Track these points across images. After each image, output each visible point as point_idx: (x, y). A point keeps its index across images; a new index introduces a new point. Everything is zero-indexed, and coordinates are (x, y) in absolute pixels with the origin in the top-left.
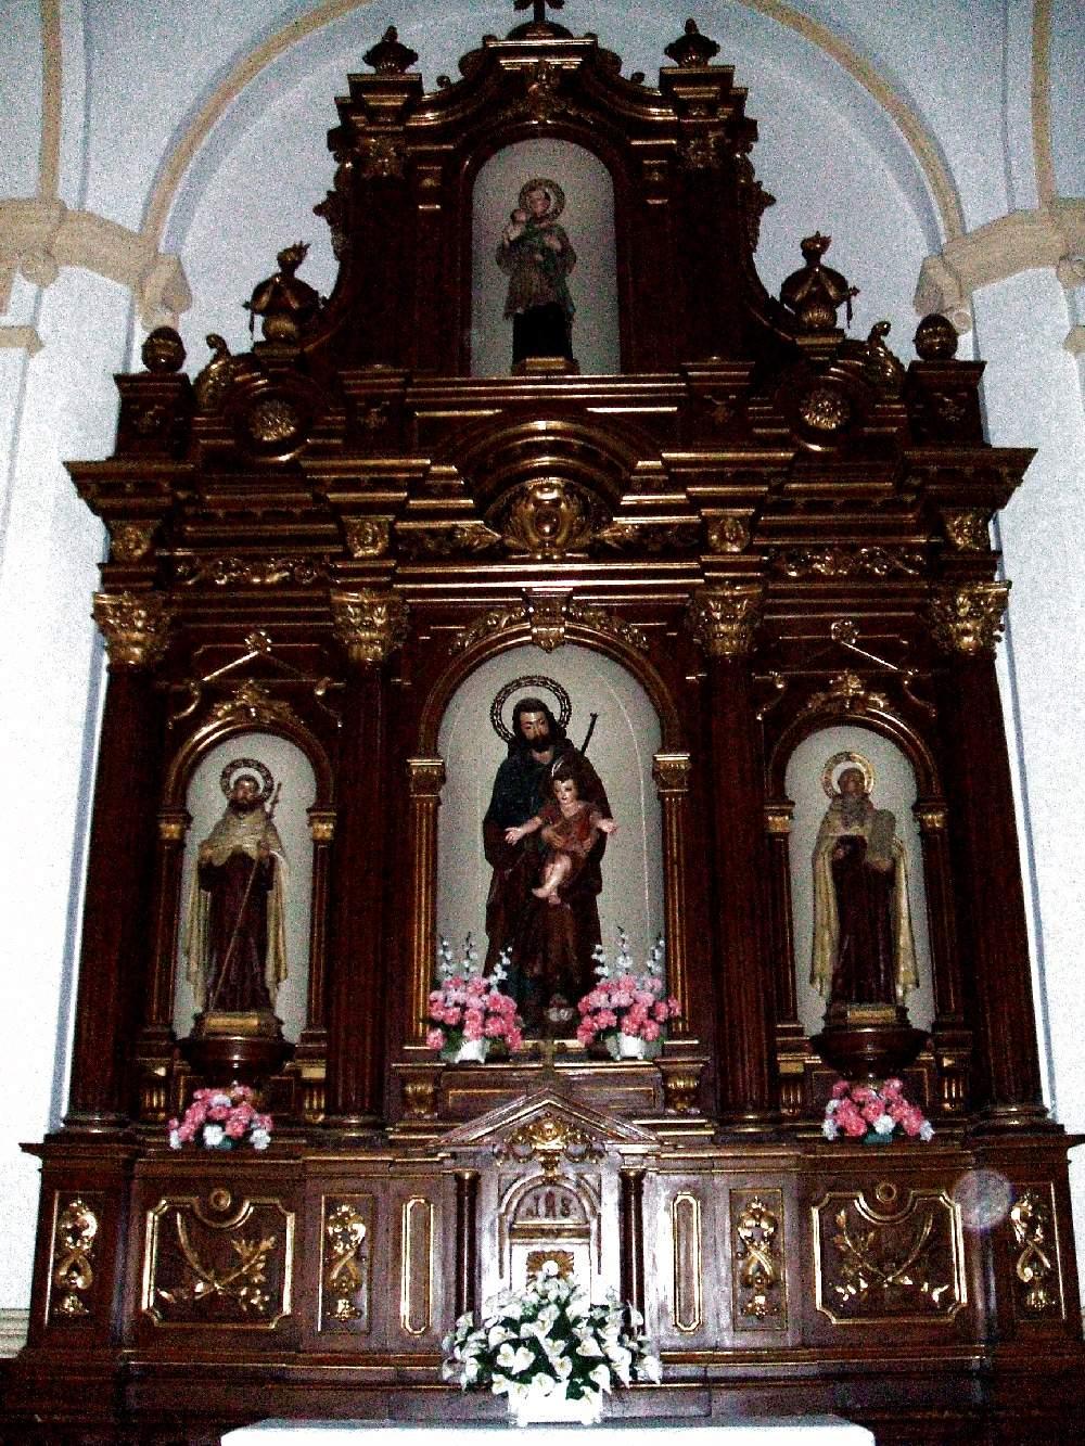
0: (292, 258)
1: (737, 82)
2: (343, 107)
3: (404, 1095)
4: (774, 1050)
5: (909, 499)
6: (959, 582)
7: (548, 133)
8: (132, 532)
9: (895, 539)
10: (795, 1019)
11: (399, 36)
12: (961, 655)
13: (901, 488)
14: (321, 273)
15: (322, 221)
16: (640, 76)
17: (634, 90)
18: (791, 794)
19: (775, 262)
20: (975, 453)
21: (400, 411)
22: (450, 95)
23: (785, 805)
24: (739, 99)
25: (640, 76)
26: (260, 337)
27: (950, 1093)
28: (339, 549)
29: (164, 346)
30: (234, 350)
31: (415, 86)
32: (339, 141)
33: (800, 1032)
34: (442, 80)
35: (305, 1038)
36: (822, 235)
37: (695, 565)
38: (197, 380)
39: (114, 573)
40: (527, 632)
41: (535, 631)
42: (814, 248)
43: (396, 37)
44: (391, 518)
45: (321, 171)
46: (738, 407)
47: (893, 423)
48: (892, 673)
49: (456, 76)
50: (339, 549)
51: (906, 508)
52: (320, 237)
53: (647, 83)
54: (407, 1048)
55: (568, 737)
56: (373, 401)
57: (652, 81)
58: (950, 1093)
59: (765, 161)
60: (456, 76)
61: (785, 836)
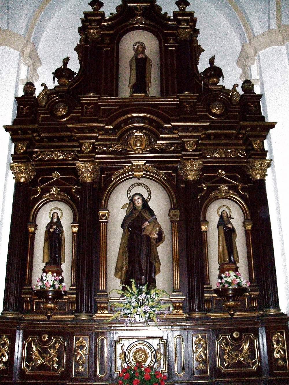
0: (66, 61)
2: (83, 21)
3: (97, 307)
4: (203, 292)
5: (241, 136)
7: (143, 29)
8: (20, 145)
9: (237, 147)
10: (209, 284)
12: (257, 180)
13: (239, 133)
14: (75, 66)
15: (76, 53)
16: (166, 13)
18: (207, 219)
19: (203, 66)
20: (261, 123)
21: (97, 107)
22: (113, 17)
23: (206, 222)
24: (195, 21)
25: (166, 13)
26: (57, 84)
28: (79, 149)
29: (29, 87)
30: (49, 88)
31: (103, 15)
32: (81, 30)
33: (211, 288)
34: (111, 14)
35: (70, 289)
37: (181, 155)
38: (38, 96)
39: (16, 157)
40: (133, 174)
41: (135, 173)
42: (212, 61)
44: (94, 141)
45: (76, 39)
46: (194, 107)
47: (236, 111)
48: (237, 184)
49: (115, 12)
50: (79, 149)
51: (239, 139)
53: (168, 15)
55: (79, 43)
56: (89, 104)
57: (170, 15)
59: (201, 39)
60: (115, 12)
61: (206, 232)
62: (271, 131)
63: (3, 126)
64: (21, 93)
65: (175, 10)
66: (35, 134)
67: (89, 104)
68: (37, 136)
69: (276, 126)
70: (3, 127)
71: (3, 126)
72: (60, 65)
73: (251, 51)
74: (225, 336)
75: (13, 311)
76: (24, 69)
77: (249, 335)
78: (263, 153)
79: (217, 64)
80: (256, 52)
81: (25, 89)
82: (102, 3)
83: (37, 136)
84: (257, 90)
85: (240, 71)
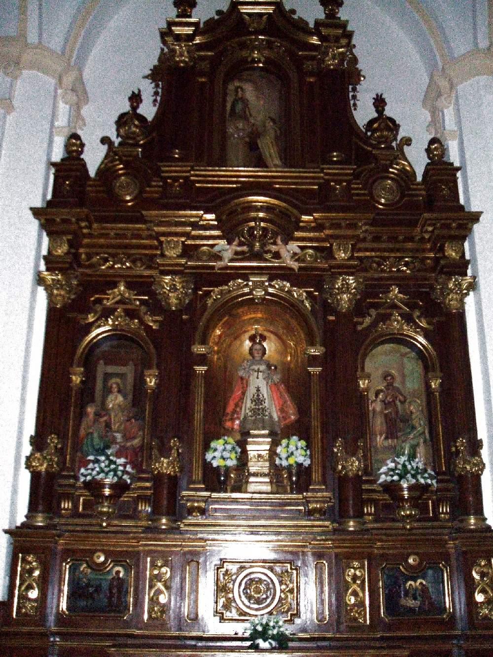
1: (349, 28)
6: (450, 275)
11: (223, 10)
14: (148, 110)
17: (301, 25)
19: (364, 113)
27: (443, 510)
36: (152, 68)
42: (379, 103)
43: (223, 11)
52: (148, 89)
54: (146, 617)
58: (443, 510)
62: (476, 227)
63: (31, 209)
64: (58, 155)
65: (320, 18)
66: (83, 224)
67: (175, 179)
68: (86, 227)
69: (481, 219)
70: (30, 212)
71: (31, 209)
72: (126, 107)
73: (443, 84)
74: (397, 564)
75: (43, 512)
76: (63, 108)
77: (397, 564)
78: (461, 266)
79: (388, 112)
80: (452, 86)
81: (67, 146)
82: (211, 19)
83: (86, 227)
84: (454, 157)
85: (427, 116)
